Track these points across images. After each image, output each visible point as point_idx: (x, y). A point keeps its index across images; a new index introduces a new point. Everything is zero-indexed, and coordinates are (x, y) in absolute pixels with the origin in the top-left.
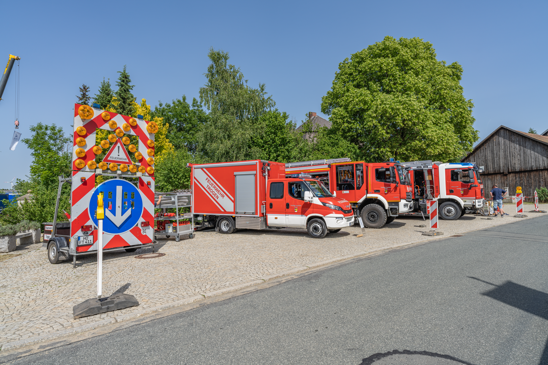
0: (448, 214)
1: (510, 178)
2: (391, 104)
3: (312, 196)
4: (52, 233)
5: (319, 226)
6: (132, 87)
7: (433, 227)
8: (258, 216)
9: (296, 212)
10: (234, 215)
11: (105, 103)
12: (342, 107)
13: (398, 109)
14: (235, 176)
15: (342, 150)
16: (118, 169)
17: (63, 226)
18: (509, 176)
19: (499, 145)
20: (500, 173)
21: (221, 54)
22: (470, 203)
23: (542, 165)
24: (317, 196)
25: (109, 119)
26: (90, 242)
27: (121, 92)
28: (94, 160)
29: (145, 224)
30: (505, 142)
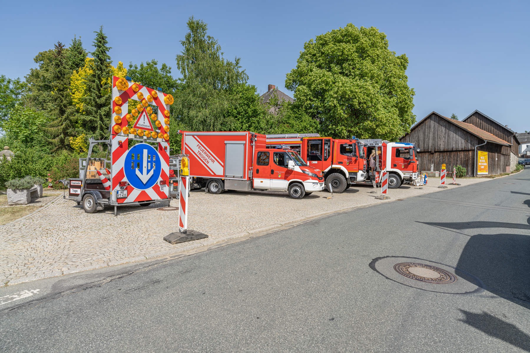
0: (391, 184)
1: (435, 156)
2: (350, 87)
3: (294, 165)
4: (82, 188)
5: (298, 189)
6: (109, 49)
7: (383, 193)
8: (246, 179)
9: (280, 177)
10: (223, 178)
11: (77, 61)
12: (306, 85)
13: (356, 92)
14: (226, 144)
15: (305, 124)
16: (144, 135)
17: (91, 182)
18: (435, 155)
19: (430, 128)
20: (428, 152)
21: (200, 23)
22: (408, 176)
23: (460, 147)
24: (298, 165)
25: (138, 90)
26: (125, 195)
27: (99, 53)
28: (127, 126)
29: (163, 183)
30: (434, 126)
